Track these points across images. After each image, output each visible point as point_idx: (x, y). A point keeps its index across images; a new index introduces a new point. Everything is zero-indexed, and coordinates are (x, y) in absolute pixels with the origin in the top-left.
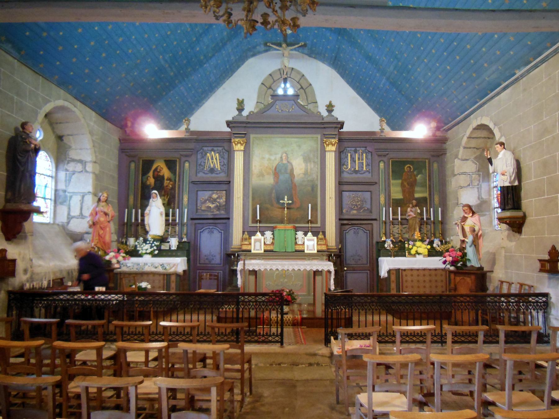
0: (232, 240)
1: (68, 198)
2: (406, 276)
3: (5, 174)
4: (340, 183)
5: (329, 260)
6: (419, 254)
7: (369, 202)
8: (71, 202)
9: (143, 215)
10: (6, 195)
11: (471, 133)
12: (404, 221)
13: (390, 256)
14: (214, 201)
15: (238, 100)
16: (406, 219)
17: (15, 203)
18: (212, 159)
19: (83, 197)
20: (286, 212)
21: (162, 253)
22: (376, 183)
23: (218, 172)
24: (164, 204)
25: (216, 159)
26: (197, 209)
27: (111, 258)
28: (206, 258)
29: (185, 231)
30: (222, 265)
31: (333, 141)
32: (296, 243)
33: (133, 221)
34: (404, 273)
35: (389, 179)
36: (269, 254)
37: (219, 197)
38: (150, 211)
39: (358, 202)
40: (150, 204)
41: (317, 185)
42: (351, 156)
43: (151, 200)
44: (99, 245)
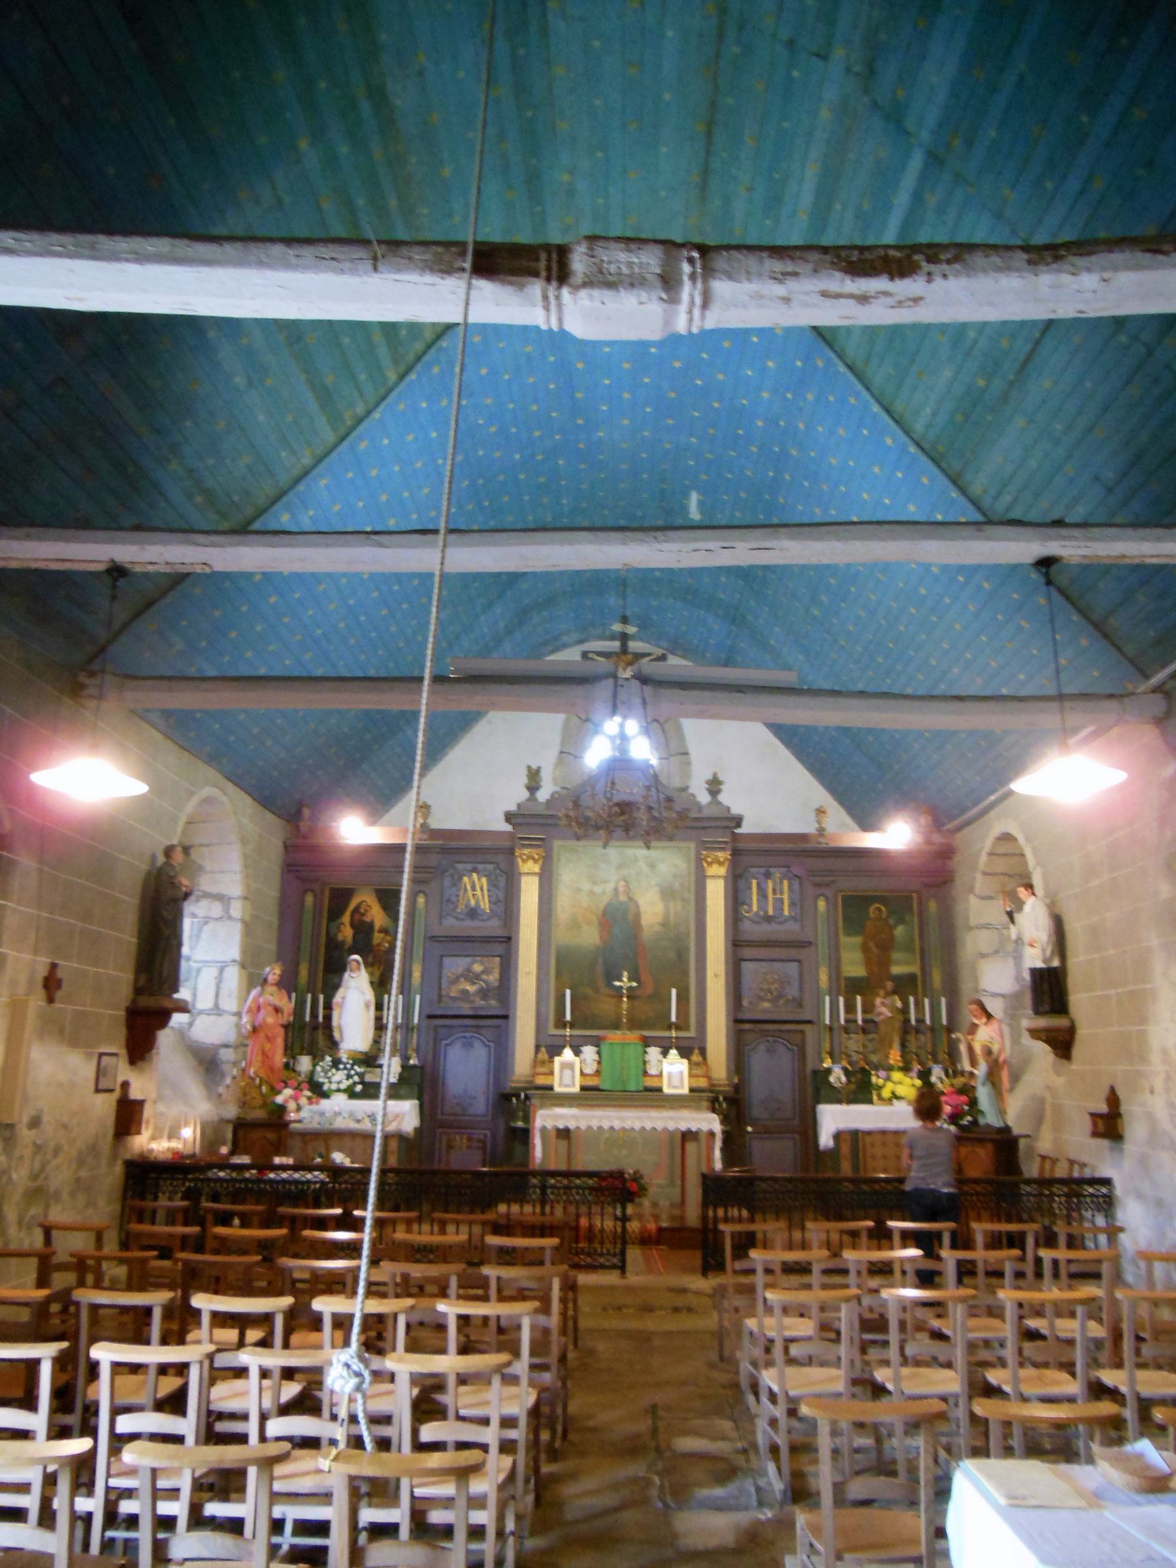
0: (513, 1065)
1: (194, 974)
2: (872, 1145)
3: (135, 940)
4: (737, 943)
5: (714, 1110)
6: (898, 1098)
7: (796, 984)
8: (199, 980)
9: (328, 1007)
10: (136, 980)
11: (994, 845)
12: (870, 1026)
13: (839, 1102)
14: (474, 978)
15: (529, 767)
16: (873, 1022)
17: (151, 995)
18: (473, 888)
19: (222, 970)
20: (625, 1006)
21: (370, 1091)
22: (810, 943)
23: (485, 917)
24: (372, 983)
25: (482, 889)
26: (440, 996)
27: (286, 1101)
28: (455, 1101)
29: (415, 1041)
30: (489, 1118)
31: (721, 855)
32: (645, 1073)
33: (307, 1018)
34: (868, 1139)
35: (836, 934)
36: (591, 1094)
37: (487, 970)
38: (343, 998)
39: (773, 983)
40: (344, 983)
41: (688, 949)
42: (758, 884)
43: (346, 975)
44: (262, 1074)
